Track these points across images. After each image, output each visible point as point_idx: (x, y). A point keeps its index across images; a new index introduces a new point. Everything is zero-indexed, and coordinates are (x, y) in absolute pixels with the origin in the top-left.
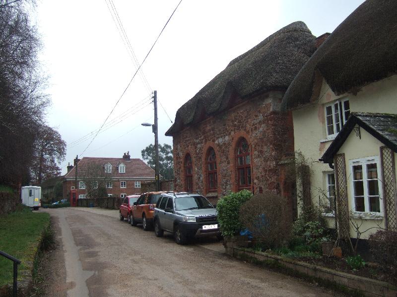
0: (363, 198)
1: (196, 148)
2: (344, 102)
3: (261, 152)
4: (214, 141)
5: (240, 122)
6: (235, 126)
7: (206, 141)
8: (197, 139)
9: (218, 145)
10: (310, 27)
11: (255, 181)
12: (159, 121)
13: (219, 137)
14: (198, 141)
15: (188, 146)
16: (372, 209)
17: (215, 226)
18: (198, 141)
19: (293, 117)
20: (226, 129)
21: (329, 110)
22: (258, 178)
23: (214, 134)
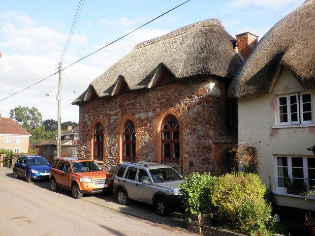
0: (286, 106)
1: (109, 118)
2: (303, 95)
3: (194, 130)
4: (133, 114)
5: (167, 100)
6: (161, 103)
7: (123, 114)
8: (110, 111)
9: (139, 119)
10: (286, 191)
11: (186, 156)
12: (110, 226)
13: (140, 112)
14: (112, 113)
15: (98, 117)
16: (293, 120)
17: (131, 140)
18: (112, 113)
19: (238, 104)
20: (150, 105)
21: (283, 101)
22: (188, 153)
23: (134, 108)
